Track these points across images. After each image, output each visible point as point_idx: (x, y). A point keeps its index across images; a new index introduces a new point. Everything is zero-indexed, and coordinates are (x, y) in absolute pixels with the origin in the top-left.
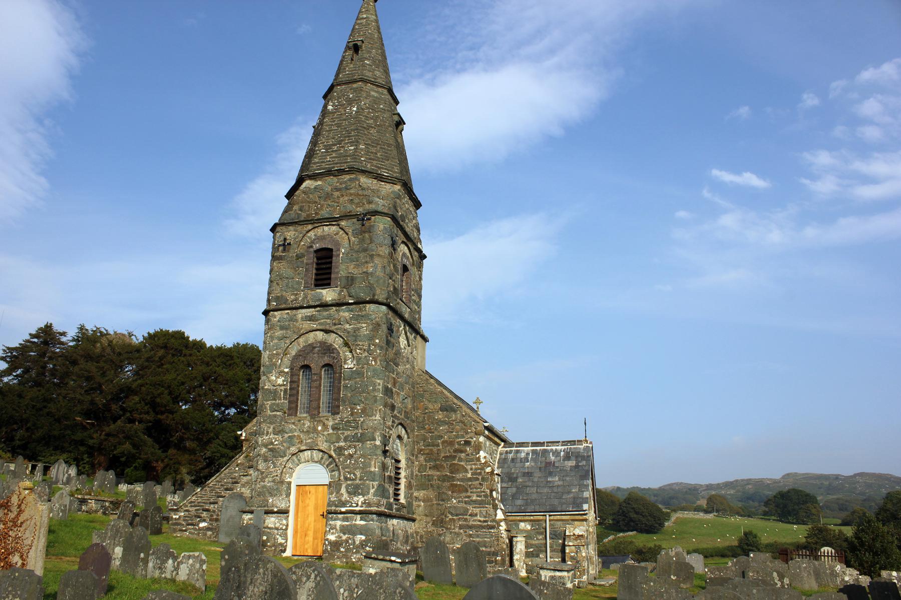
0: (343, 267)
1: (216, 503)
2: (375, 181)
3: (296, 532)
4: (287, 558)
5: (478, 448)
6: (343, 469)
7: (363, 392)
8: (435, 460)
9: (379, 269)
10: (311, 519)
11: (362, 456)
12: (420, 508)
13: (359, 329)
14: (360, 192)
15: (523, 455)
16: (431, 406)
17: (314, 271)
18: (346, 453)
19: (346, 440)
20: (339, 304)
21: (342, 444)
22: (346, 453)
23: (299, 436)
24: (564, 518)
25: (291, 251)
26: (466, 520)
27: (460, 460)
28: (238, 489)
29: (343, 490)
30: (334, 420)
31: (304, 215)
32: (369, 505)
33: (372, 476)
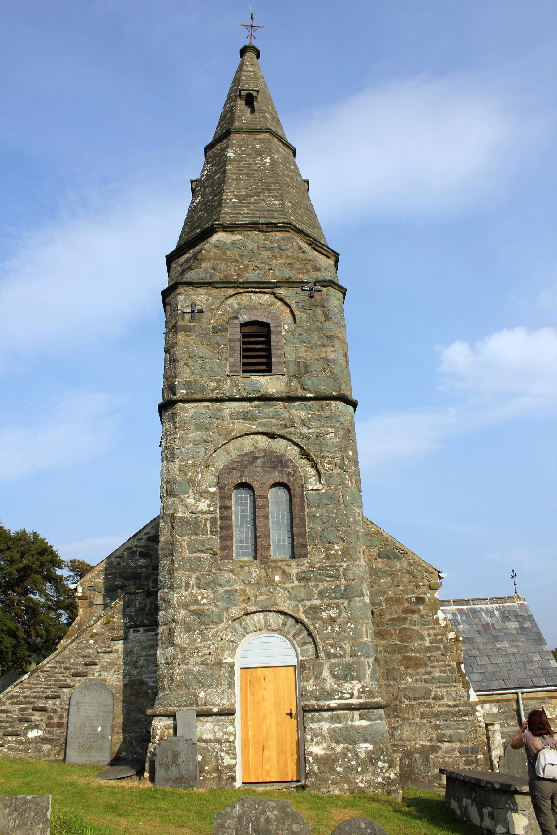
1: (59, 697)
3: (245, 744)
6: (323, 640)
10: (271, 722)
18: (324, 615)
19: (321, 595)
21: (316, 602)
22: (324, 615)
24: (540, 695)
28: (96, 673)
29: (326, 674)
31: (218, 277)
32: (371, 694)
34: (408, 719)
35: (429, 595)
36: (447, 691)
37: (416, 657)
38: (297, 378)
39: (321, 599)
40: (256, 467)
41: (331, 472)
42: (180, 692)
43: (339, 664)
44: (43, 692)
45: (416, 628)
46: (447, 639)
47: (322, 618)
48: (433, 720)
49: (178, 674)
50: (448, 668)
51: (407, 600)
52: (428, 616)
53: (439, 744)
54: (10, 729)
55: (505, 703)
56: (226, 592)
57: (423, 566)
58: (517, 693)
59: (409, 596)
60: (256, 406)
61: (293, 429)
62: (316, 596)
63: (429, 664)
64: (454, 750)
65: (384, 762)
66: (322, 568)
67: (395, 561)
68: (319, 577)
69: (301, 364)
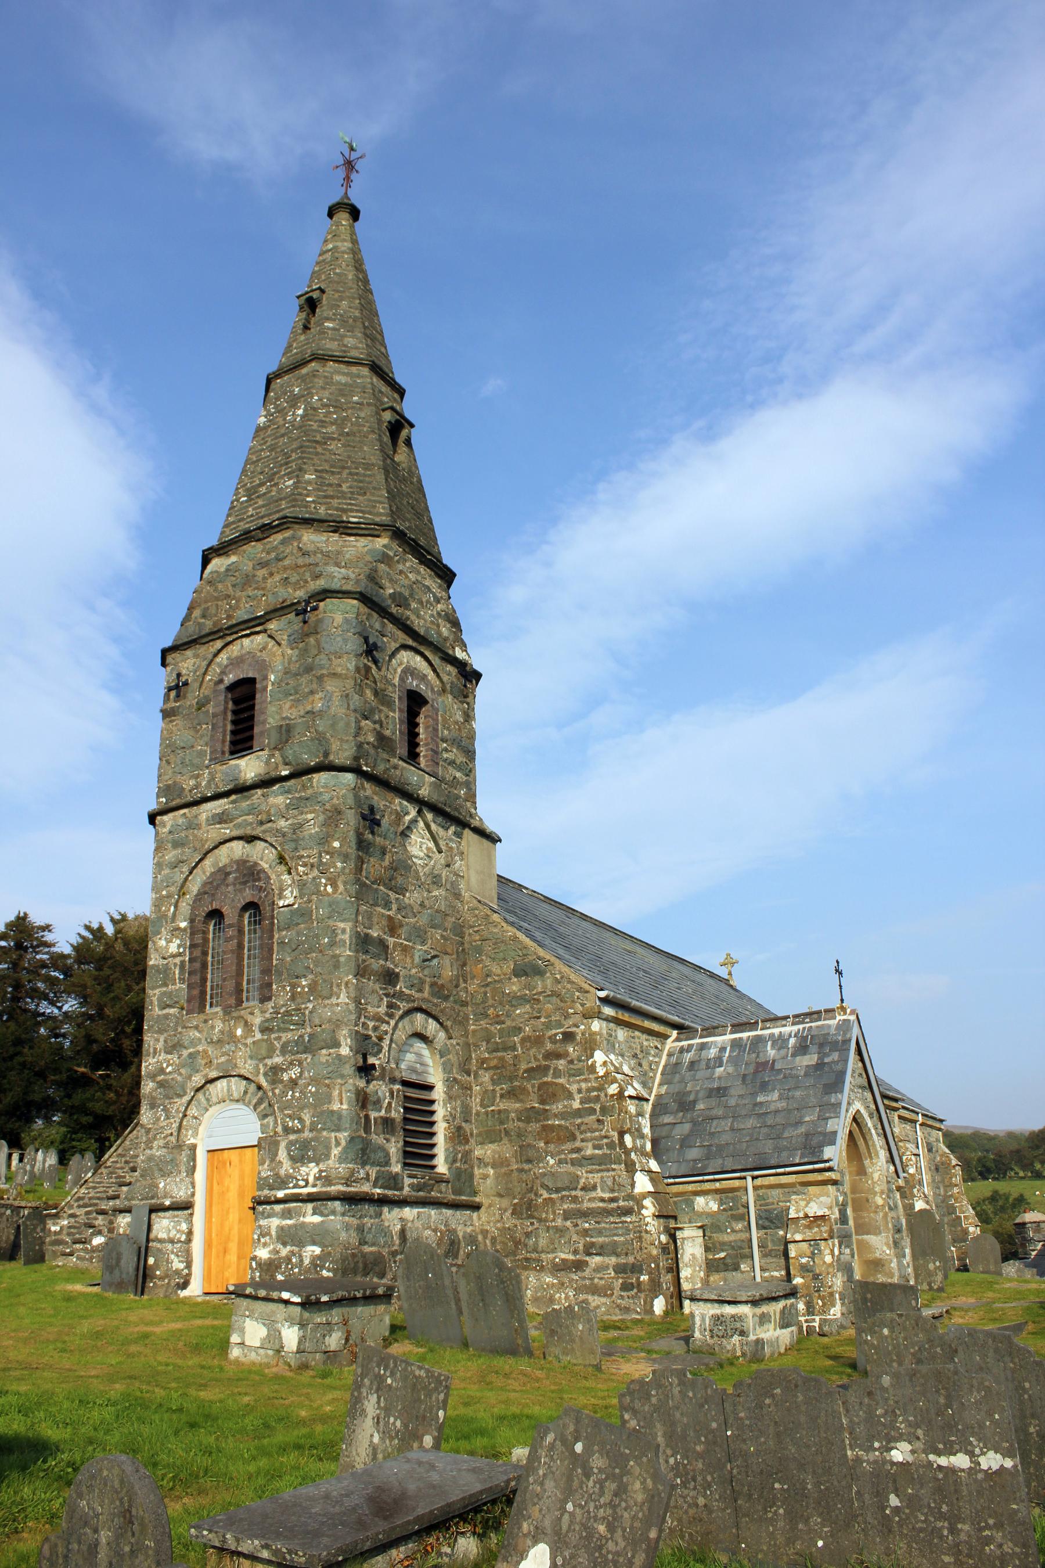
0: (272, 709)
2: (335, 537)
3: (208, 1245)
4: (185, 1301)
5: (590, 1045)
6: (281, 1110)
7: (311, 950)
8: (511, 1079)
9: (336, 700)
10: (233, 1217)
11: (313, 1081)
12: (486, 1181)
13: (301, 825)
14: (300, 561)
15: (713, 1052)
16: (495, 969)
17: (229, 727)
19: (284, 1051)
20: (266, 783)
21: (278, 1060)
22: (285, 1077)
23: (205, 1052)
24: (784, 1179)
25: (189, 695)
26: (575, 1200)
27: (557, 1073)
29: (282, 1155)
30: (263, 1012)
31: (209, 625)
32: (328, 1181)
33: (334, 1121)
34: (546, 1220)
35: (582, 1027)
36: (602, 1177)
37: (559, 1125)
38: (279, 750)
39: (284, 1056)
40: (227, 885)
41: (305, 877)
42: (144, 1183)
43: (297, 1141)
44: (105, 1192)
45: (561, 1081)
46: (606, 1095)
47: (282, 1081)
48: (579, 1222)
49: (143, 1162)
50: (605, 1141)
51: (550, 1038)
52: (580, 1061)
53: (587, 1258)
54: (77, 1236)
55: (730, 1195)
56: (190, 1054)
57: (574, 983)
58: (745, 1178)
59: (554, 1031)
60: (233, 802)
61: (269, 825)
62: (278, 1052)
63: (579, 1137)
64: (607, 1267)
65: (329, 1271)
66: (288, 1013)
67: (536, 979)
68: (282, 1025)
69: (284, 728)
